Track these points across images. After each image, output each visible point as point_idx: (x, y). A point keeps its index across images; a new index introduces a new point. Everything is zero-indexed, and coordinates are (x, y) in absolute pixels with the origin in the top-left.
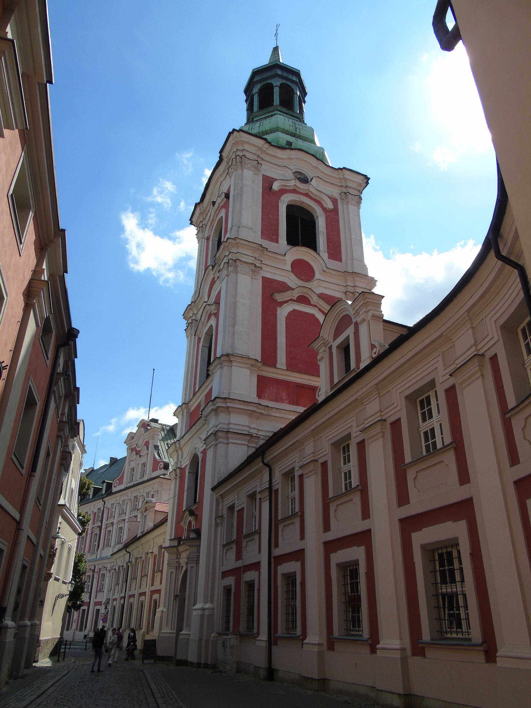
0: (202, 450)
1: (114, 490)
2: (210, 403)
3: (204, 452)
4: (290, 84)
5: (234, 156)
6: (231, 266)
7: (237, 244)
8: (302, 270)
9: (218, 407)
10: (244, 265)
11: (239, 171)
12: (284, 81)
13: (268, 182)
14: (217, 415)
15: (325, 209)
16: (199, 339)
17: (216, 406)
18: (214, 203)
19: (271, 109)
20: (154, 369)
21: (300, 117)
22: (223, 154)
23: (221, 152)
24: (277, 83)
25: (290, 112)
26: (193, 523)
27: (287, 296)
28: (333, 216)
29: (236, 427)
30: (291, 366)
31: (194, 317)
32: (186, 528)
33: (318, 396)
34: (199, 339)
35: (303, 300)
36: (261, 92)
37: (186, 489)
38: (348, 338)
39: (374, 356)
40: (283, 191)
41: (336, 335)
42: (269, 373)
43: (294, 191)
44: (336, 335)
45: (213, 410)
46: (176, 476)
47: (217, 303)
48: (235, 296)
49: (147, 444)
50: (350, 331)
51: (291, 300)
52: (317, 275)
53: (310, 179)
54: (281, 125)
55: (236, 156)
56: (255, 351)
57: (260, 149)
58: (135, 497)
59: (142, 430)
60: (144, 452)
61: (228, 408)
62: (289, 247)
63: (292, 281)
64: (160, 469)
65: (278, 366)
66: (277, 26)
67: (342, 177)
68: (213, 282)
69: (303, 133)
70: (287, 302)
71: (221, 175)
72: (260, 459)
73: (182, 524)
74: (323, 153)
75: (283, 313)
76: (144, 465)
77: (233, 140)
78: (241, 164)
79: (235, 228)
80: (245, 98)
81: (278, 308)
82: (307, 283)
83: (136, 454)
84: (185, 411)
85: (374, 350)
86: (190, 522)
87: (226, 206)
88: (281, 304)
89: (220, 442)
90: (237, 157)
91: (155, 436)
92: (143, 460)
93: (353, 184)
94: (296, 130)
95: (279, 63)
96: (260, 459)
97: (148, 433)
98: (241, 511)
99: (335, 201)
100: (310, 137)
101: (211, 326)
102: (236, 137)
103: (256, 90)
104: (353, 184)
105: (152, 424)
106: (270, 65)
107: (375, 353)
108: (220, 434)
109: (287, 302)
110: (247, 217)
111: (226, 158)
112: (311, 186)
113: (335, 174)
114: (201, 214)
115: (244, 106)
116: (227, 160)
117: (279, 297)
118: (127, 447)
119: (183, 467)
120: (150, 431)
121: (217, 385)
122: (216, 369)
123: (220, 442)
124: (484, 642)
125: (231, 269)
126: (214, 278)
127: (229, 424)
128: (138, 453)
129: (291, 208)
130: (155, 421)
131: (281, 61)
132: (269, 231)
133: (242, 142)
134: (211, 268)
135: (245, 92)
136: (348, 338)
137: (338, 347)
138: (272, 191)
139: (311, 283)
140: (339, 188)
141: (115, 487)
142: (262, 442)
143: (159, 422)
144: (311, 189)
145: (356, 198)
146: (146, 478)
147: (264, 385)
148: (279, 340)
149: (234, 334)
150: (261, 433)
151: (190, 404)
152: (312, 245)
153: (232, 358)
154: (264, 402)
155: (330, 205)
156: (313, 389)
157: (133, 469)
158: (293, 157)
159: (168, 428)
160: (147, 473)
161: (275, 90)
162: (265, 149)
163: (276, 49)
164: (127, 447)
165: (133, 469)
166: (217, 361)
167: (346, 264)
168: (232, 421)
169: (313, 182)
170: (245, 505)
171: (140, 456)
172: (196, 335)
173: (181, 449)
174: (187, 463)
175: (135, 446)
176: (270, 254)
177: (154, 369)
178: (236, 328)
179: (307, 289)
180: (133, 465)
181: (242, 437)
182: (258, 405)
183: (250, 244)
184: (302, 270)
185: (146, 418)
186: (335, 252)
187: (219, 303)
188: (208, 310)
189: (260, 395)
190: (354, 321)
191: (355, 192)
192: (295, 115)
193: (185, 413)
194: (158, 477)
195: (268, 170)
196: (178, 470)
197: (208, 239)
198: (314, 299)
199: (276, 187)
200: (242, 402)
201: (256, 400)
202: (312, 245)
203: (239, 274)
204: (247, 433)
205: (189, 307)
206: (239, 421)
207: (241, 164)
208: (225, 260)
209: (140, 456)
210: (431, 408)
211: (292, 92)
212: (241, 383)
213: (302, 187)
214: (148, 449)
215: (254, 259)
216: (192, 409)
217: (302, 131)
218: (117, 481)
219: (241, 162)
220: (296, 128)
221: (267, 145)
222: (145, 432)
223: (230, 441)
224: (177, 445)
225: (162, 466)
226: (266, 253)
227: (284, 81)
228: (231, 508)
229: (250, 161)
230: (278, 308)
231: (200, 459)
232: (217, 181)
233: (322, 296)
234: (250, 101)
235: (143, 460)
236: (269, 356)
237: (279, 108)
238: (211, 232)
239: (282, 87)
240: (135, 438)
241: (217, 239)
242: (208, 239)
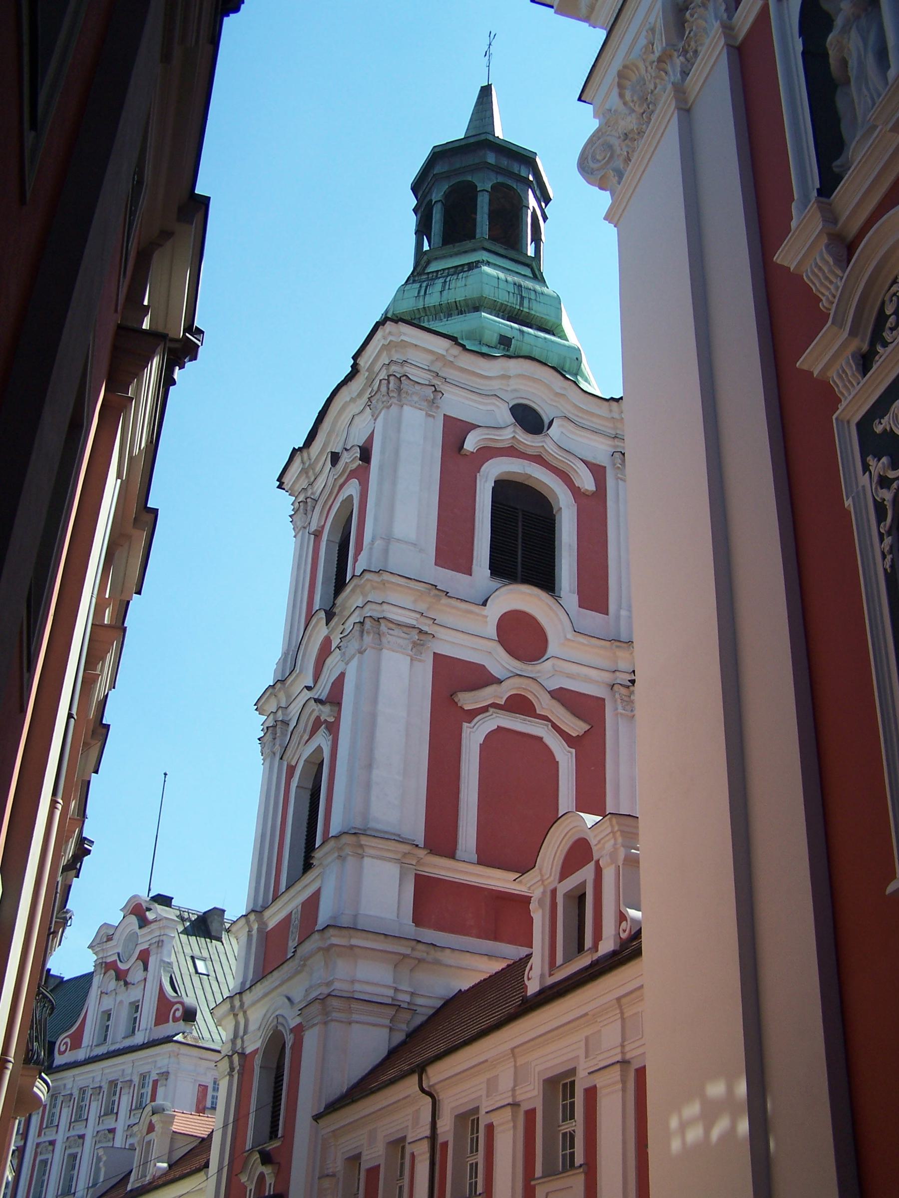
0: (293, 1023)
1: (59, 1060)
2: (316, 936)
3: (299, 1031)
4: (510, 182)
5: (383, 375)
6: (368, 633)
7: (383, 583)
8: (522, 637)
9: (333, 945)
10: (397, 632)
11: (394, 409)
12: (501, 179)
13: (455, 432)
15: (576, 492)
16: (291, 770)
17: (329, 942)
18: (335, 458)
19: (469, 244)
20: (165, 774)
22: (361, 362)
23: (355, 357)
24: (485, 183)
25: (512, 254)
26: (270, 1180)
30: (486, 858)
31: (280, 712)
32: (253, 1187)
33: (529, 979)
34: (291, 770)
35: (519, 705)
37: (253, 1108)
38: (584, 884)
39: (624, 936)
40: (487, 452)
41: (564, 874)
42: (441, 868)
43: (512, 451)
44: (564, 874)
45: (320, 949)
46: (232, 1069)
47: (334, 699)
48: (375, 701)
49: (144, 957)
50: (586, 873)
51: (494, 705)
52: (552, 650)
53: (546, 422)
54: (489, 292)
55: (389, 376)
56: (415, 826)
57: (440, 357)
58: (111, 1082)
59: (133, 919)
60: (136, 975)
61: (352, 947)
62: (495, 584)
63: (498, 661)
64: (175, 1020)
65: (459, 854)
66: (492, 36)
67: (616, 416)
68: (325, 650)
69: (538, 310)
70: (484, 710)
71: (353, 400)
72: (415, 1078)
73: (244, 1179)
74: (578, 360)
75: (473, 737)
76: (136, 1007)
77: (384, 338)
78: (399, 394)
79: (378, 542)
81: (465, 725)
82: (530, 668)
83: (118, 978)
84: (255, 927)
85: (624, 924)
86: (262, 1177)
87: (361, 473)
88: (472, 715)
89: (332, 1020)
90: (392, 378)
91: (164, 938)
92: (134, 994)
94: (521, 304)
95: (491, 138)
96: (415, 1078)
97: (145, 930)
98: (373, 1171)
99: (598, 472)
100: (552, 319)
101: (319, 749)
102: (390, 333)
103: (437, 195)
105: (160, 909)
106: (472, 140)
107: (624, 931)
108: (335, 1003)
109: (484, 710)
110: (404, 511)
111: (367, 370)
112: (548, 440)
113: (603, 410)
114: (304, 471)
115: (412, 221)
117: (468, 700)
118: (95, 957)
119: (248, 1051)
120: (153, 926)
121: (328, 881)
122: (330, 859)
125: (368, 639)
126: (327, 641)
127: (353, 982)
128: (121, 976)
129: (504, 489)
130: (164, 900)
131: (499, 132)
132: (452, 551)
133: (404, 345)
134: (322, 614)
135: (412, 189)
136: (584, 884)
137: (567, 896)
138: (463, 452)
139: (538, 667)
140: (610, 442)
141: (61, 1053)
142: (418, 1020)
143: (174, 902)
144: (551, 448)
146: (139, 1038)
148: (463, 795)
149: (368, 786)
150: (419, 1001)
151: (267, 914)
152: (546, 581)
153: (364, 840)
154: (429, 935)
155: (587, 483)
156: (682, 63)
157: (108, 1015)
158: (512, 373)
159: (193, 918)
160: (143, 1025)
161: (479, 199)
162: (451, 359)
163: (486, 92)
164: (95, 957)
165: (108, 1015)
166: (331, 844)
167: (618, 617)
168: (360, 975)
170: (382, 1162)
171: (126, 984)
172: (285, 758)
173: (245, 1012)
174: (258, 1045)
175: (115, 957)
176: (454, 602)
177: (165, 774)
178: (375, 772)
179: (530, 681)
180: (108, 1003)
181: (376, 1008)
182: (414, 943)
183: (412, 584)
185: (144, 894)
186: (594, 596)
187: (339, 704)
188: (313, 710)
189: (418, 920)
190: (595, 858)
192: (521, 259)
193: (255, 932)
194: (169, 1040)
195: (458, 404)
196: (236, 1058)
197: (317, 535)
198: (545, 704)
199: (471, 443)
200: (382, 937)
201: (408, 926)
202: (546, 581)
203: (385, 651)
204: (389, 1001)
205: (270, 690)
206: (372, 976)
207: (399, 394)
208: (356, 618)
209: (126, 984)
210: (574, 1152)
212: (381, 890)
213: (527, 441)
214: (146, 969)
215: (418, 616)
216: (271, 924)
217: (535, 306)
218: (68, 1040)
219: (399, 390)
220: (522, 298)
221: (456, 350)
222: (140, 927)
223: (355, 1017)
224: (237, 1003)
225: (179, 1014)
226: (445, 600)
227: (501, 179)
228: (355, 1159)
229: (418, 387)
230: (465, 725)
231: (288, 1045)
232: (344, 408)
233: (561, 696)
234: (423, 213)
235: (134, 994)
236: (440, 837)
237: (487, 245)
238: (325, 520)
240: (115, 937)
241: (337, 538)
242: (317, 535)
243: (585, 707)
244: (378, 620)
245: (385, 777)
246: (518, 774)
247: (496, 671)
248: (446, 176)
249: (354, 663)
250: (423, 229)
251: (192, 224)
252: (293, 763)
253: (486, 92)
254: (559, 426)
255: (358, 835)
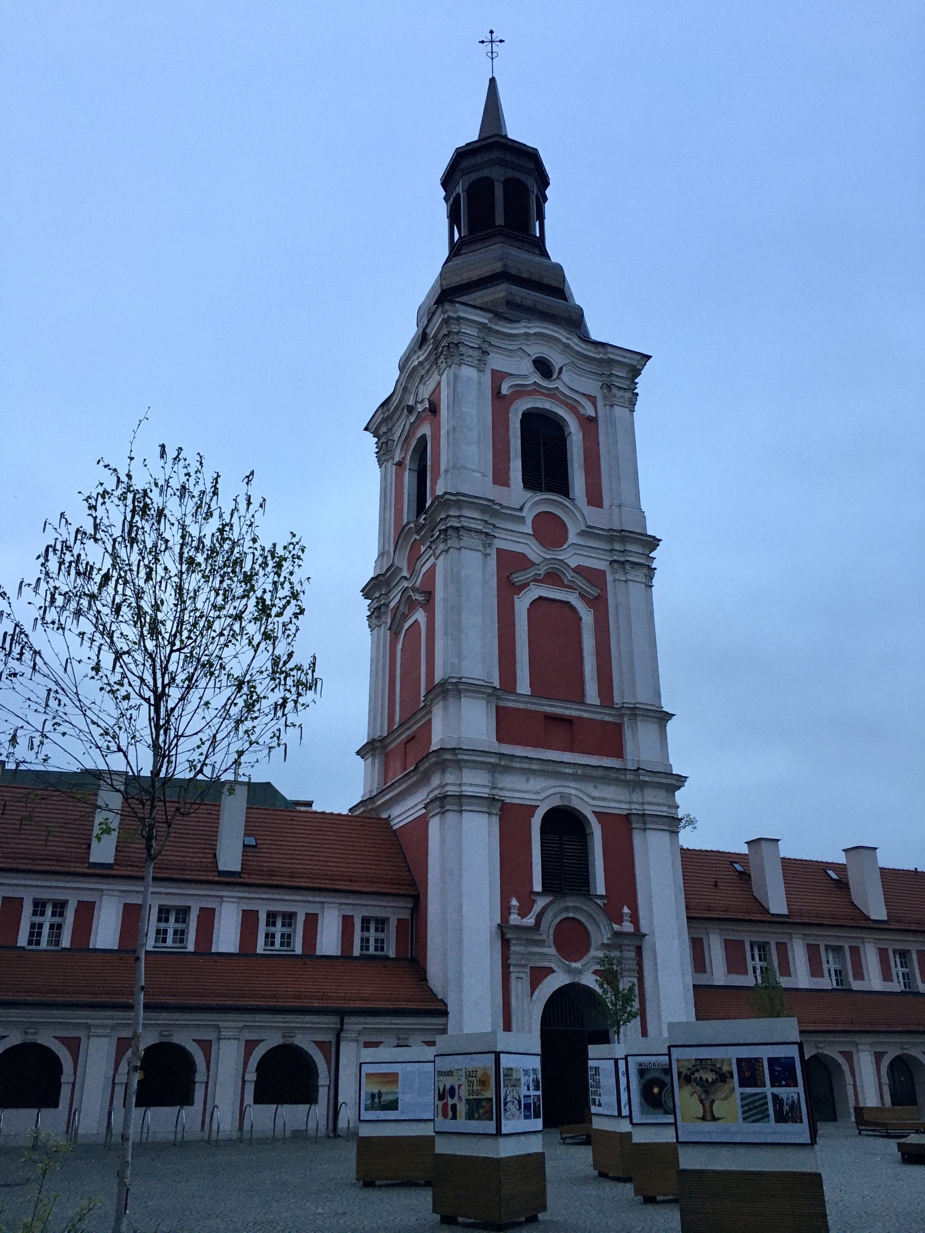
8: (550, 531)
13: (498, 377)
14: (443, 772)
21: (539, 246)
27: (531, 573)
28: (589, 424)
29: (471, 789)
35: (553, 577)
36: (471, 190)
40: (520, 392)
43: (536, 390)
52: (572, 538)
62: (529, 494)
63: (533, 551)
75: (522, 604)
80: (444, 193)
81: (516, 597)
93: (621, 371)
104: (621, 371)
116: (435, 344)
117: (518, 578)
123: (449, 810)
124: (509, 966)
127: (460, 785)
129: (529, 418)
145: (628, 395)
147: (508, 725)
154: (507, 749)
163: (493, 81)
168: (465, 780)
169: (564, 375)
181: (480, 801)
184: (550, 531)
186: (595, 498)
189: (499, 739)
191: (624, 384)
195: (497, 361)
211: (524, 191)
227: (510, 173)
239: (509, 183)
243: (595, 577)
244: (457, 345)
245: (467, 640)
246: (555, 624)
247: (533, 557)
248: (466, 172)
249: (444, 376)
250: (454, 217)
251: (55, 1105)
252: (377, 1183)
253: (493, 81)
254: (567, 371)
255: (458, 500)
